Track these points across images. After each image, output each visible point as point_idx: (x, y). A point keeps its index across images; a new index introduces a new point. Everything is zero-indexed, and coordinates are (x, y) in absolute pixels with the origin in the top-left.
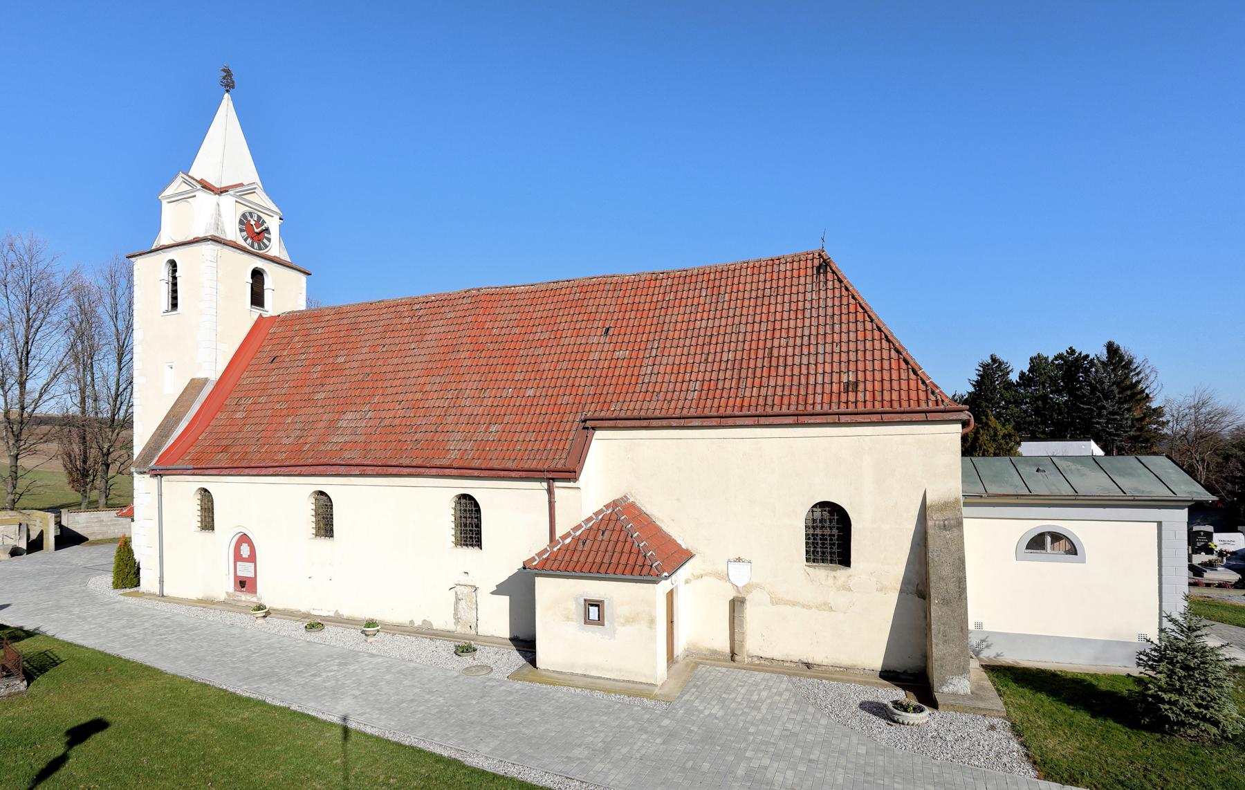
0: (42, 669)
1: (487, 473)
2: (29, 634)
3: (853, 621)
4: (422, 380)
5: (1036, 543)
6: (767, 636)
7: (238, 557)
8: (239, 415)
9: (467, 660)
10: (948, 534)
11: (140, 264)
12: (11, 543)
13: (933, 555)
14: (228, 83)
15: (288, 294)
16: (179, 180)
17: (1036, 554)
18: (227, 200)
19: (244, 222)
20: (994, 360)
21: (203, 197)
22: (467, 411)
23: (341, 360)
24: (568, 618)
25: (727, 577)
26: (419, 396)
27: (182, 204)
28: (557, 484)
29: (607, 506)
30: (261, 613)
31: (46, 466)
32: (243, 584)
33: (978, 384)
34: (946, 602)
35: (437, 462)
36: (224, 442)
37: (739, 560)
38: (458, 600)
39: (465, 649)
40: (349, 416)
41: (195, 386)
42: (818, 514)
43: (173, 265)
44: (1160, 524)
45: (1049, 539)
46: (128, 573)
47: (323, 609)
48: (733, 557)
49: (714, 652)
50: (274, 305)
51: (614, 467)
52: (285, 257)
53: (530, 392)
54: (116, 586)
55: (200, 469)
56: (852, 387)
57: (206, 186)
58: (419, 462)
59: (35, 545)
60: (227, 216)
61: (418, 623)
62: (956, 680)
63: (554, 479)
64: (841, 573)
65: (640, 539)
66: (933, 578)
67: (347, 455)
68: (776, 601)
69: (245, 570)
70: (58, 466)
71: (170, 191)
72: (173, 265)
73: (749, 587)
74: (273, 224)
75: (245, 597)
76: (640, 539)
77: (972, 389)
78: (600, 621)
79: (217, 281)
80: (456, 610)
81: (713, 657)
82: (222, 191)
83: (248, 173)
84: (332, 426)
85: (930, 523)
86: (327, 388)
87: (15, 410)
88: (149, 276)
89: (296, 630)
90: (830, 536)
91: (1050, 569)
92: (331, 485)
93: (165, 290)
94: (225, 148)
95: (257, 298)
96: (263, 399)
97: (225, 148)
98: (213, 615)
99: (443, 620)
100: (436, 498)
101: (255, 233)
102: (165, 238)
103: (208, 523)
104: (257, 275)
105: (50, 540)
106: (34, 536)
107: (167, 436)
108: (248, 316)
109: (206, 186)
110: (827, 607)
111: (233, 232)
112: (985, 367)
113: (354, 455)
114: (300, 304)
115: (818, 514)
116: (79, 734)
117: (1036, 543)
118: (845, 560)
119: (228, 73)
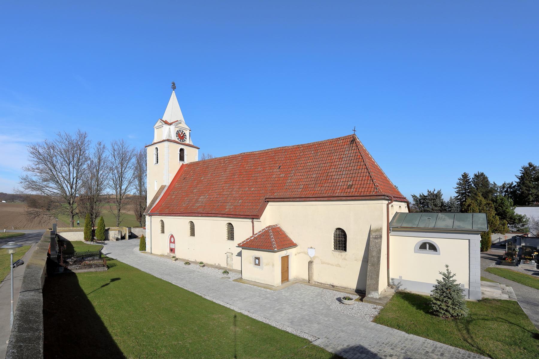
0: (112, 267)
1: (234, 216)
2: (113, 259)
3: (344, 271)
4: (223, 185)
5: (423, 246)
6: (322, 275)
7: (171, 242)
8: (173, 197)
9: (225, 275)
10: (376, 241)
11: (149, 149)
12: (116, 236)
13: (371, 248)
14: (174, 87)
15: (192, 156)
16: (159, 122)
17: (424, 251)
18: (172, 127)
19: (178, 134)
20: (531, 165)
21: (166, 127)
22: (234, 196)
23: (202, 178)
24: (251, 263)
25: (307, 254)
26: (222, 190)
27: (160, 129)
28: (254, 220)
29: (266, 228)
30: (174, 259)
31: (130, 212)
32: (172, 250)
33: (522, 178)
34: (373, 265)
35: (222, 213)
36: (168, 206)
37: (311, 248)
38: (227, 257)
39: (226, 272)
40: (202, 197)
41: (162, 188)
42: (338, 233)
43: (157, 148)
44: (469, 240)
45: (428, 245)
46: (143, 247)
47: (192, 259)
48: (310, 247)
49: (304, 280)
50: (187, 161)
51: (274, 214)
52: (191, 143)
53: (253, 189)
54: (140, 250)
55: (161, 214)
56: (350, 187)
57: (166, 123)
58: (217, 212)
59: (123, 238)
60: (170, 132)
61: (217, 264)
62: (373, 293)
63: (253, 218)
64: (344, 253)
65: (272, 238)
66: (370, 256)
67: (199, 210)
68: (323, 263)
69: (172, 246)
70: (132, 213)
71: (156, 126)
72: (157, 148)
73: (315, 257)
74: (187, 133)
75: (172, 255)
76: (272, 238)
77: (518, 180)
78: (259, 264)
79: (169, 152)
80: (227, 260)
81: (303, 281)
82: (171, 124)
83: (179, 116)
84: (197, 201)
85: (371, 236)
86: (198, 188)
87: (119, 196)
88: (151, 152)
89: (182, 264)
90: (341, 241)
91: (428, 256)
92: (195, 219)
93: (155, 157)
94: (173, 110)
95: (182, 158)
96: (180, 192)
97: (173, 110)
98: (162, 259)
99: (224, 265)
100: (221, 223)
101: (181, 136)
102: (155, 141)
103: (163, 232)
104: (182, 150)
105: (127, 237)
106: (123, 235)
107: (154, 204)
108: (178, 164)
109: (166, 123)
110: (339, 266)
111: (174, 137)
112: (525, 169)
113: (200, 210)
114: (196, 159)
115: (338, 233)
116: (113, 280)
117: (423, 246)
118: (345, 250)
119: (174, 84)
